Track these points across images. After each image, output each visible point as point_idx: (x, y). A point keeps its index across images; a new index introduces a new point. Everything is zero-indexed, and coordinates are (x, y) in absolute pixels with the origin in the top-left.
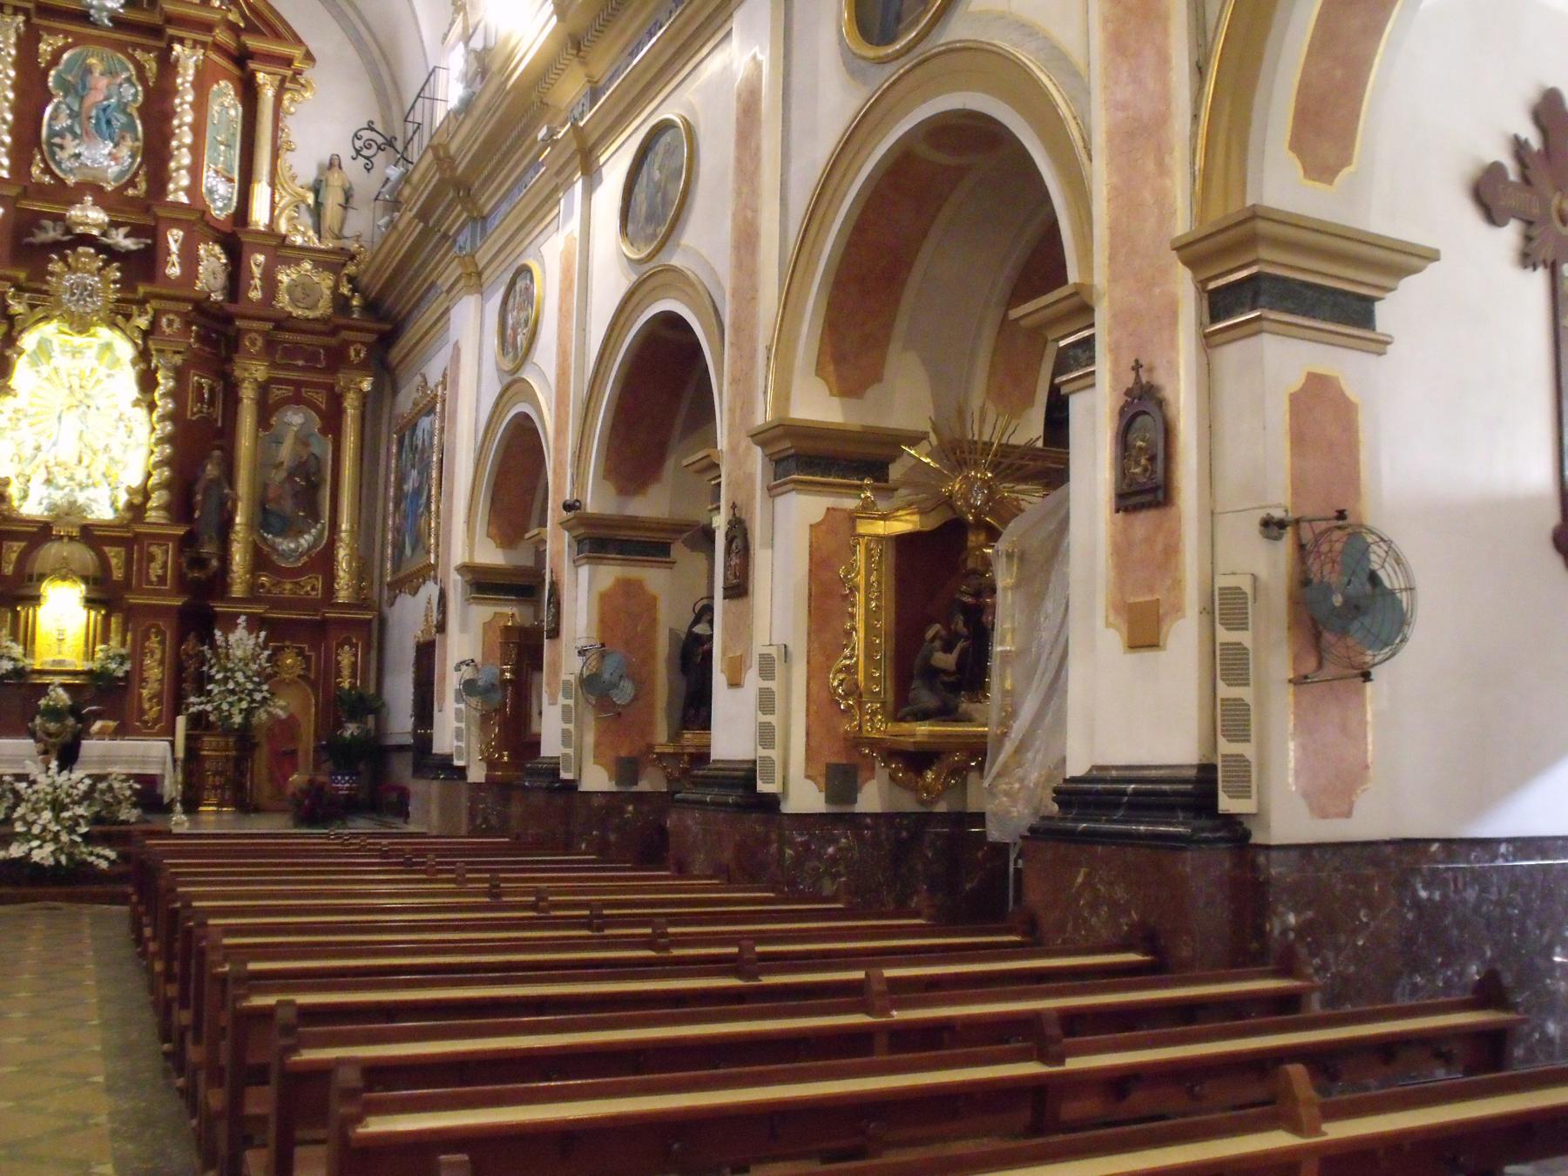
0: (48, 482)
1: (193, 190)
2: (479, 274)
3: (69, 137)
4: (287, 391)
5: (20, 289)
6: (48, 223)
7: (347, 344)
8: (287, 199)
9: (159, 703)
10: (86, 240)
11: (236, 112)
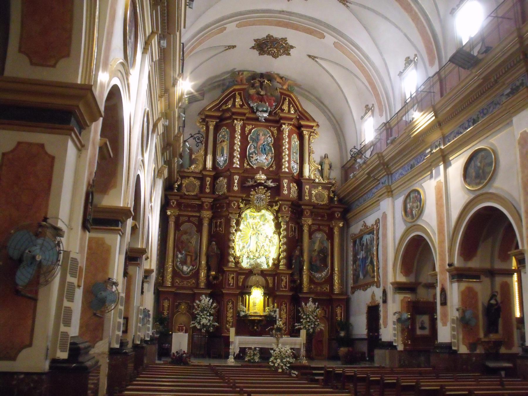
0: (248, 257)
1: (289, 168)
2: (392, 191)
4: (186, 219)
6: (250, 180)
7: (334, 212)
9: (286, 325)
10: (261, 184)
11: (297, 143)
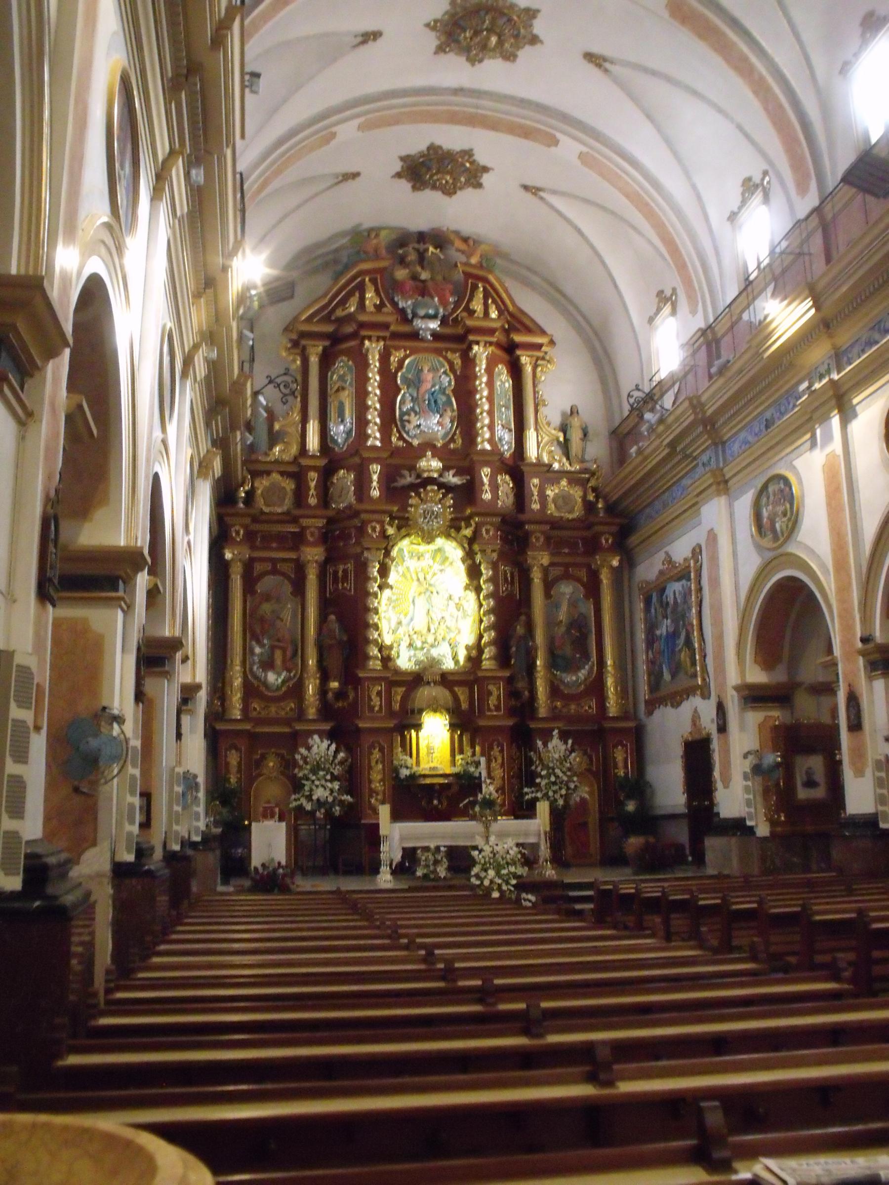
2: (726, 482)
3: (413, 414)
4: (268, 566)
5: (392, 518)
8: (546, 439)
10: (431, 481)
